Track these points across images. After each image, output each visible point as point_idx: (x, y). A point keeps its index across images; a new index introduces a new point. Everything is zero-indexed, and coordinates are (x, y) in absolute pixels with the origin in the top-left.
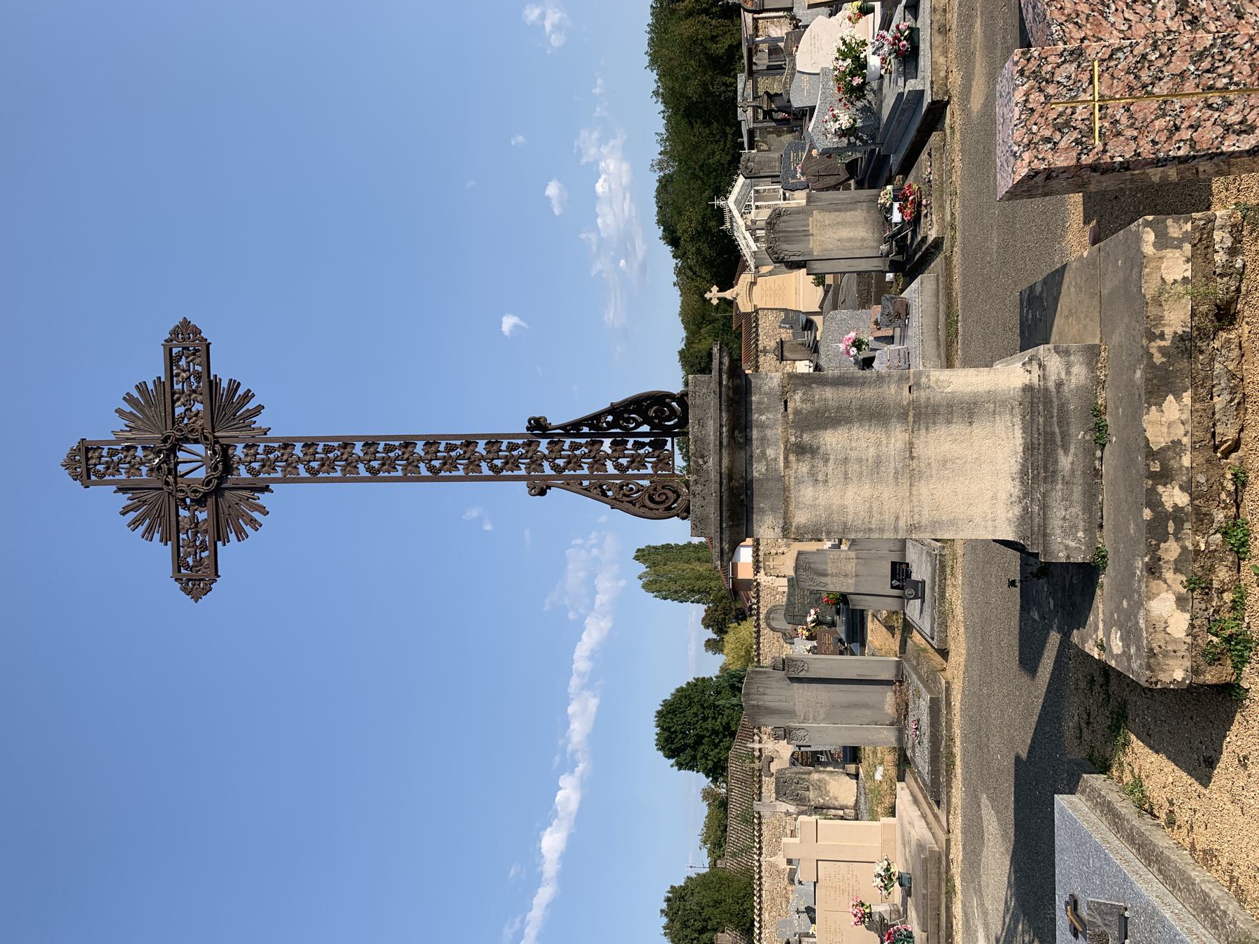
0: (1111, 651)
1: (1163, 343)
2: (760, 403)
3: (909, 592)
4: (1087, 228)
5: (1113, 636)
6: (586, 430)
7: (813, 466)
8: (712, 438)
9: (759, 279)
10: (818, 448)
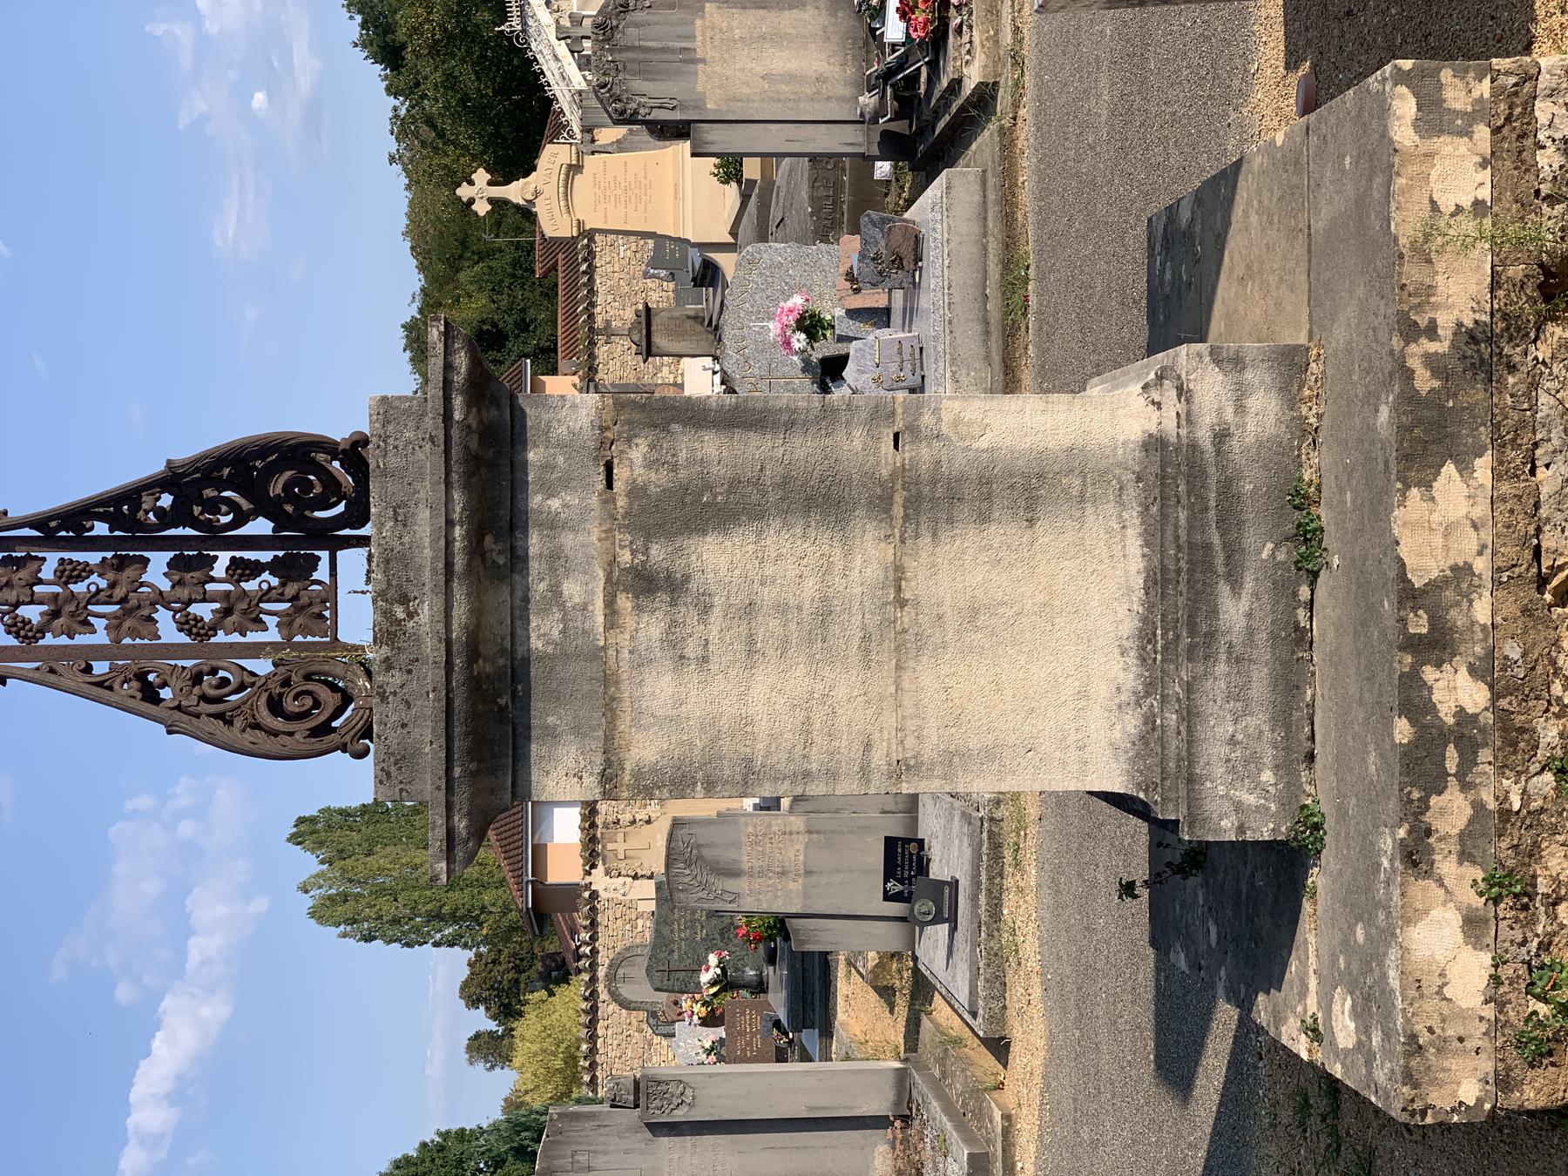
0: (1333, 1042)
1: (1433, 347)
2: (548, 467)
3: (924, 906)
4: (1293, 79)
5: (1336, 1007)
6: (101, 529)
7: (674, 623)
8: (427, 555)
9: (588, 159)
10: (687, 578)
